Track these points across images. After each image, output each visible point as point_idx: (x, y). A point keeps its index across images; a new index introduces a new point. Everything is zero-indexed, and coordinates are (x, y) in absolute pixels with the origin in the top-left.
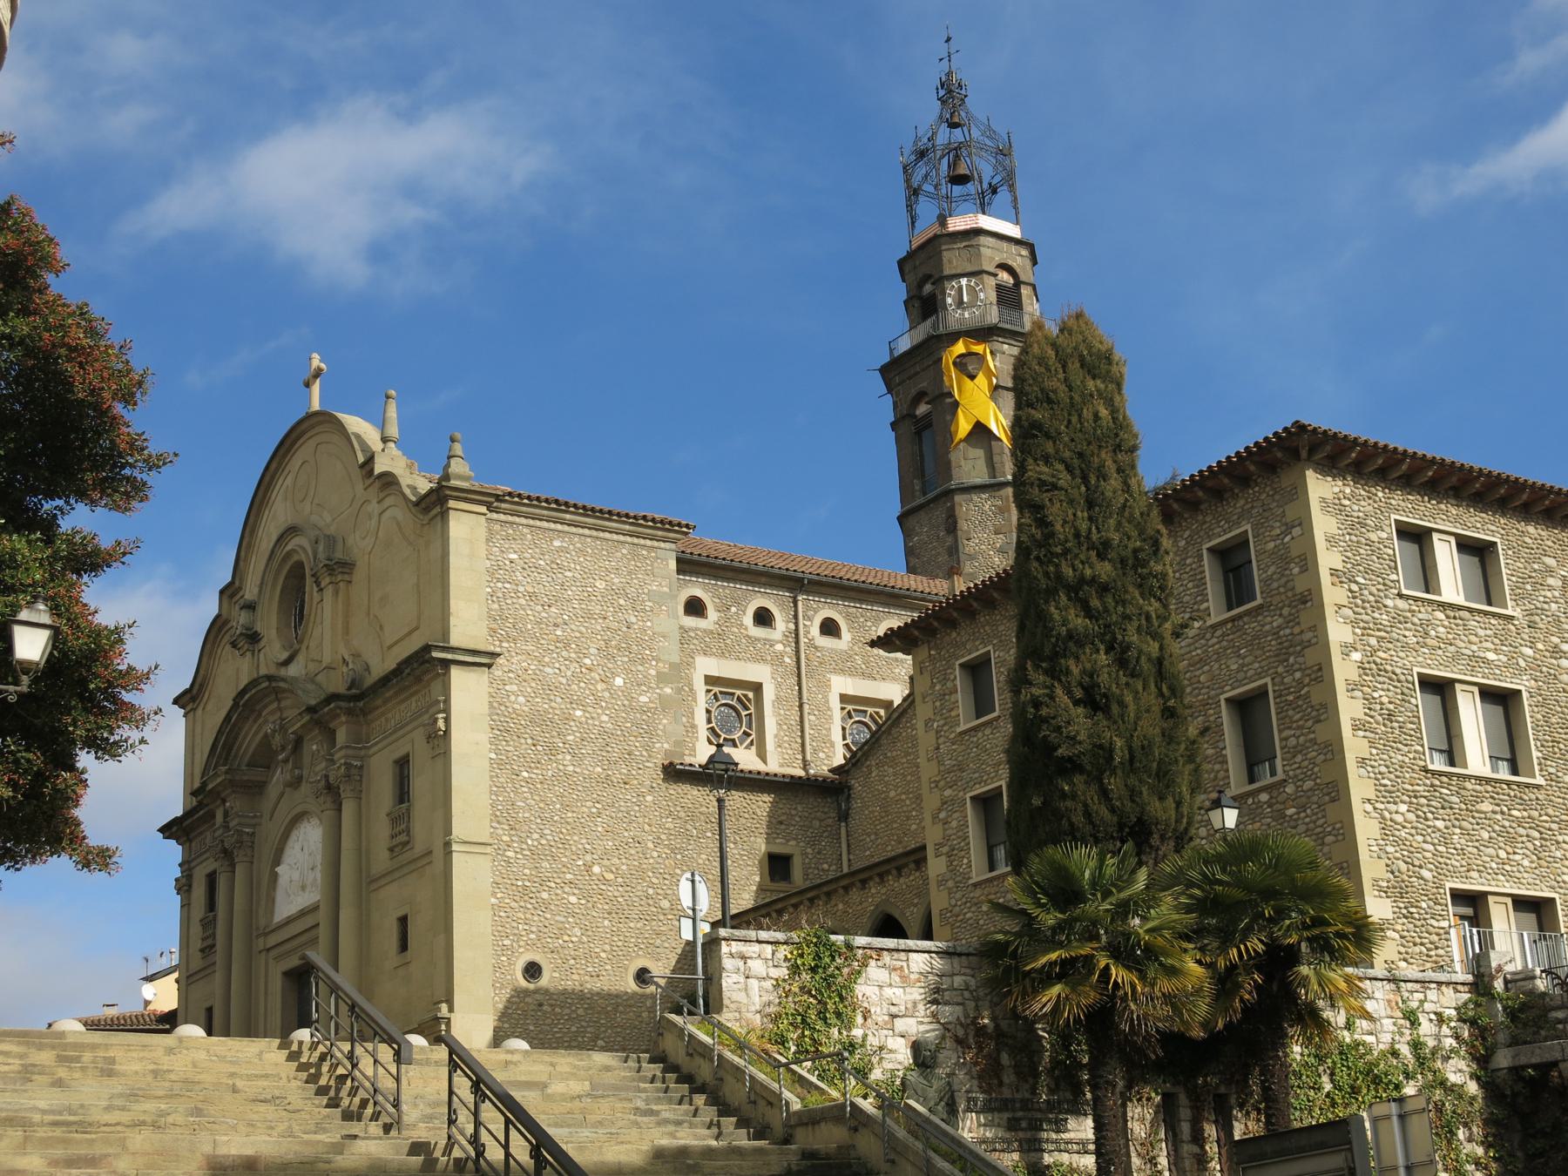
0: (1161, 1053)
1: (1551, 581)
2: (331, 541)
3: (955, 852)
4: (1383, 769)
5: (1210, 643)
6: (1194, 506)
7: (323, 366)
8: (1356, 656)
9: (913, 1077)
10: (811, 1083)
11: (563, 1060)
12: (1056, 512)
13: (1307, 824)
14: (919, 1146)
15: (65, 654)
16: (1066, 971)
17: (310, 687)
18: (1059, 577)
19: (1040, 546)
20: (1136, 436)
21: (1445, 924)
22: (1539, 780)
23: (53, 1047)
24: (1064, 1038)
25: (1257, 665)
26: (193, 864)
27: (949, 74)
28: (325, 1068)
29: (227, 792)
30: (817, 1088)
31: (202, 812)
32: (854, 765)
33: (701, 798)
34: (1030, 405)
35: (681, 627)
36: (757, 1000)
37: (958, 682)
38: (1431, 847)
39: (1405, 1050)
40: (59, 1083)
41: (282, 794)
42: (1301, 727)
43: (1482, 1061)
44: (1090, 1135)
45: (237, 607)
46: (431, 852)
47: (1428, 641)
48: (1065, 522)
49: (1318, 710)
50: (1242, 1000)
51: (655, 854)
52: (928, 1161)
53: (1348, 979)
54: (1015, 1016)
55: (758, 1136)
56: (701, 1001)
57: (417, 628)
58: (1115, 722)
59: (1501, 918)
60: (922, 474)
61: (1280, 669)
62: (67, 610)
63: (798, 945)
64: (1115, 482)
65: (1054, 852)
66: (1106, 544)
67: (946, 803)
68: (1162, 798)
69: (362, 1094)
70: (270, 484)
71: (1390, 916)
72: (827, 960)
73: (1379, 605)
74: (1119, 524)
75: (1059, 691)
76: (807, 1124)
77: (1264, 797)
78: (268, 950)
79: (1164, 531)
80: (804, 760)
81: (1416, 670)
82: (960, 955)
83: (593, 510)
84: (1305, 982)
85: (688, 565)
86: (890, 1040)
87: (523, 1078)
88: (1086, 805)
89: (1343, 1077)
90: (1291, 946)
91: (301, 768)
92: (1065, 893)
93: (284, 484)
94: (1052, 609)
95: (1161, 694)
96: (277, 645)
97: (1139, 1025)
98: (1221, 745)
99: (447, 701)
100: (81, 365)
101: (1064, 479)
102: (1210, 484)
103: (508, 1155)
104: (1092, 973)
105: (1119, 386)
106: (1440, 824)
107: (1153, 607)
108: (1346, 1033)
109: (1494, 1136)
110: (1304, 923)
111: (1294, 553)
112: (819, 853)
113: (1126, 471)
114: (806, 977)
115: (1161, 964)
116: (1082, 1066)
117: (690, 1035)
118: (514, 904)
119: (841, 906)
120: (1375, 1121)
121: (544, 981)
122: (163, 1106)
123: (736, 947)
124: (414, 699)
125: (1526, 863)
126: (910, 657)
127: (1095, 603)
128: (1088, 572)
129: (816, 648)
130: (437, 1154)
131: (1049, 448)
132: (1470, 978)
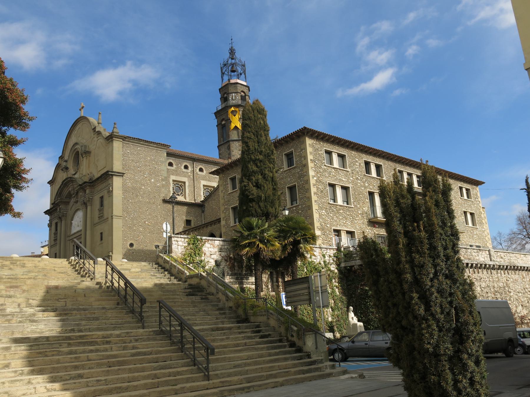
0: (270, 263)
1: (357, 164)
2: (85, 146)
4: (320, 203)
6: (282, 145)
7: (84, 106)
8: (315, 178)
9: (215, 268)
10: (191, 269)
11: (135, 264)
12: (251, 144)
14: (215, 283)
15: (7, 165)
16: (250, 245)
17: (80, 180)
18: (251, 158)
19: (247, 151)
20: (269, 128)
21: (332, 236)
22: (353, 206)
23: (10, 260)
24: (249, 259)
27: (232, 47)
28: (77, 265)
30: (193, 270)
31: (54, 208)
32: (206, 200)
33: (170, 206)
34: (246, 120)
35: (167, 169)
36: (180, 251)
37: (229, 182)
38: (329, 220)
39: (322, 263)
40: (11, 269)
41: (74, 204)
42: (303, 193)
43: (338, 265)
44: (254, 281)
47: (331, 176)
48: (253, 146)
50: (288, 252)
51: (160, 219)
52: (217, 286)
53: (311, 247)
54: (238, 255)
55: (179, 281)
56: (168, 251)
57: (105, 167)
58: (262, 191)
59: (344, 235)
60: (223, 137)
61: (299, 181)
62: (8, 154)
63: (190, 239)
64: (264, 138)
65: (247, 219)
66: (262, 151)
68: (272, 208)
69: (86, 271)
70: (71, 133)
71: (320, 234)
72: (196, 242)
73: (320, 167)
74: (265, 147)
75: (250, 184)
76: (190, 278)
77: (294, 208)
79: (274, 149)
80: (195, 199)
81: (328, 182)
82: (226, 241)
83: (147, 141)
84: (301, 248)
85: (169, 155)
86: (210, 260)
87: (125, 268)
88: (255, 209)
89: (309, 268)
90: (299, 240)
91: (78, 199)
92: (250, 228)
93: (75, 133)
94: (249, 165)
95: (273, 185)
97: (265, 257)
98: (286, 197)
99: (112, 184)
100: (11, 93)
101: (253, 137)
102: (285, 140)
103: (119, 285)
104: (255, 245)
105: (266, 116)
106: (331, 215)
107: (271, 166)
108: (310, 259)
109: (340, 281)
110: (302, 235)
111: (303, 156)
113: (267, 135)
114: (191, 246)
115: (270, 243)
116: (253, 266)
117: (164, 258)
118: (127, 230)
119: (202, 231)
120: (314, 277)
121: (134, 247)
122: (36, 274)
123: (175, 239)
124: (104, 183)
125: (349, 224)
126: (218, 177)
127: (259, 164)
128: (257, 157)
129: (198, 174)
130: (103, 285)
131: (250, 129)
132: (336, 248)
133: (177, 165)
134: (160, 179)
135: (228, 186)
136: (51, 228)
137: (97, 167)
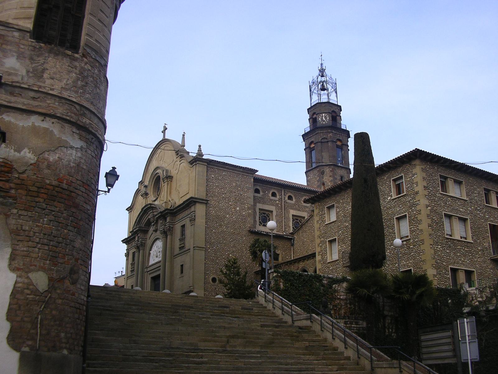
1: (475, 192)
2: (167, 171)
3: (323, 254)
5: (392, 203)
8: (429, 208)
13: (416, 250)
25: (404, 209)
26: (129, 250)
29: (139, 232)
41: (153, 233)
45: (143, 186)
46: (190, 249)
49: (419, 221)
57: (188, 193)
67: (321, 242)
78: (148, 272)
96: (152, 196)
112: (286, 254)
129: (287, 203)
133: (264, 192)
134: (246, 207)
135: (324, 215)
136: (128, 258)
137: (179, 192)
